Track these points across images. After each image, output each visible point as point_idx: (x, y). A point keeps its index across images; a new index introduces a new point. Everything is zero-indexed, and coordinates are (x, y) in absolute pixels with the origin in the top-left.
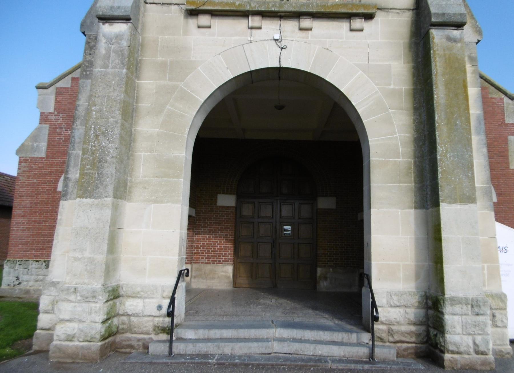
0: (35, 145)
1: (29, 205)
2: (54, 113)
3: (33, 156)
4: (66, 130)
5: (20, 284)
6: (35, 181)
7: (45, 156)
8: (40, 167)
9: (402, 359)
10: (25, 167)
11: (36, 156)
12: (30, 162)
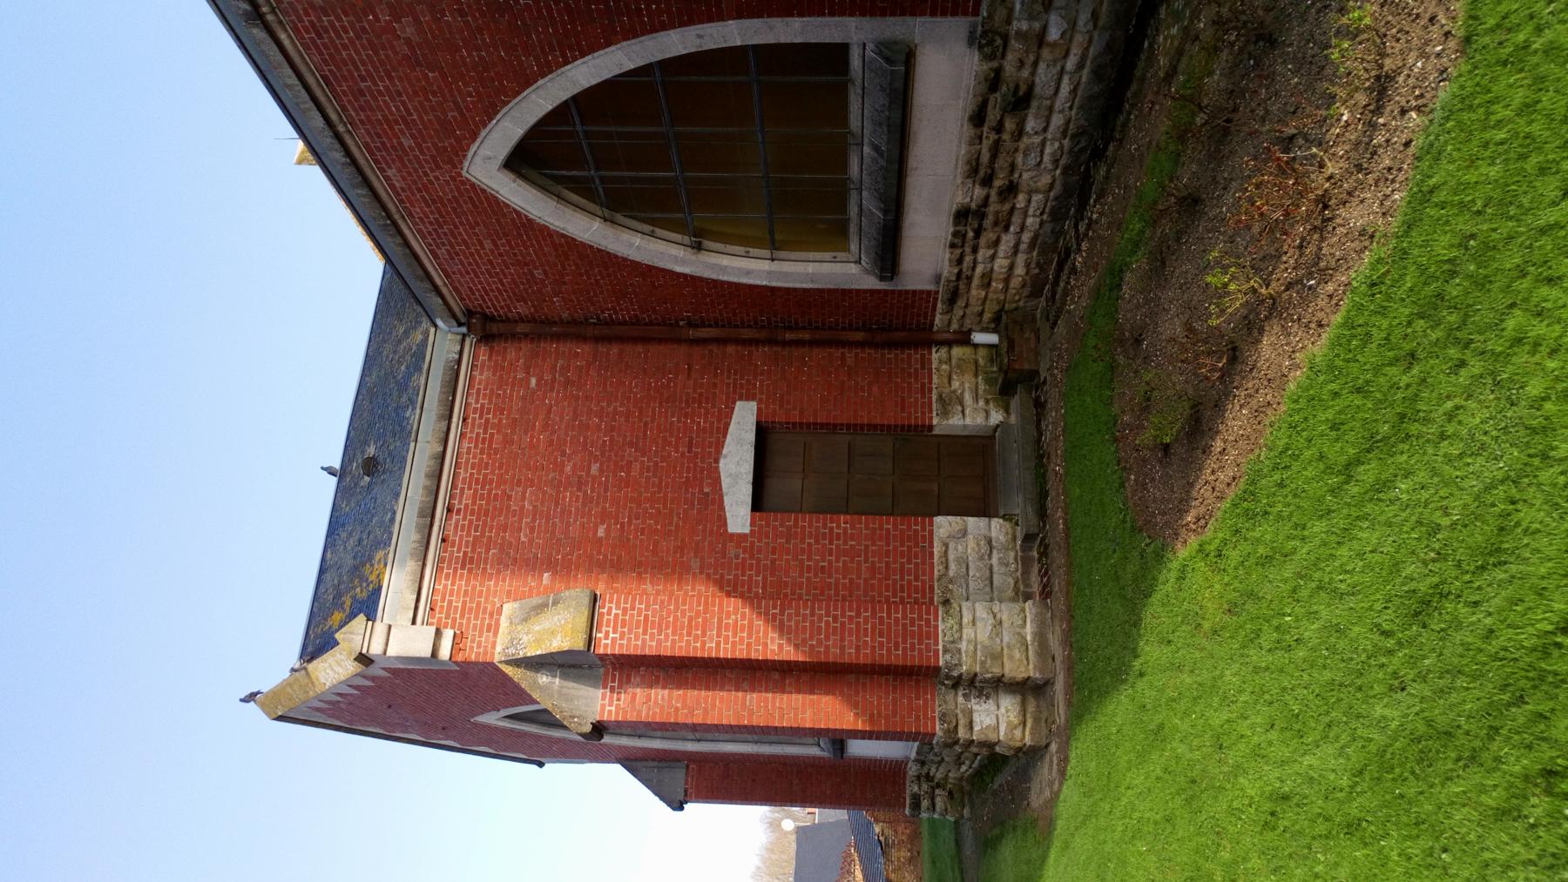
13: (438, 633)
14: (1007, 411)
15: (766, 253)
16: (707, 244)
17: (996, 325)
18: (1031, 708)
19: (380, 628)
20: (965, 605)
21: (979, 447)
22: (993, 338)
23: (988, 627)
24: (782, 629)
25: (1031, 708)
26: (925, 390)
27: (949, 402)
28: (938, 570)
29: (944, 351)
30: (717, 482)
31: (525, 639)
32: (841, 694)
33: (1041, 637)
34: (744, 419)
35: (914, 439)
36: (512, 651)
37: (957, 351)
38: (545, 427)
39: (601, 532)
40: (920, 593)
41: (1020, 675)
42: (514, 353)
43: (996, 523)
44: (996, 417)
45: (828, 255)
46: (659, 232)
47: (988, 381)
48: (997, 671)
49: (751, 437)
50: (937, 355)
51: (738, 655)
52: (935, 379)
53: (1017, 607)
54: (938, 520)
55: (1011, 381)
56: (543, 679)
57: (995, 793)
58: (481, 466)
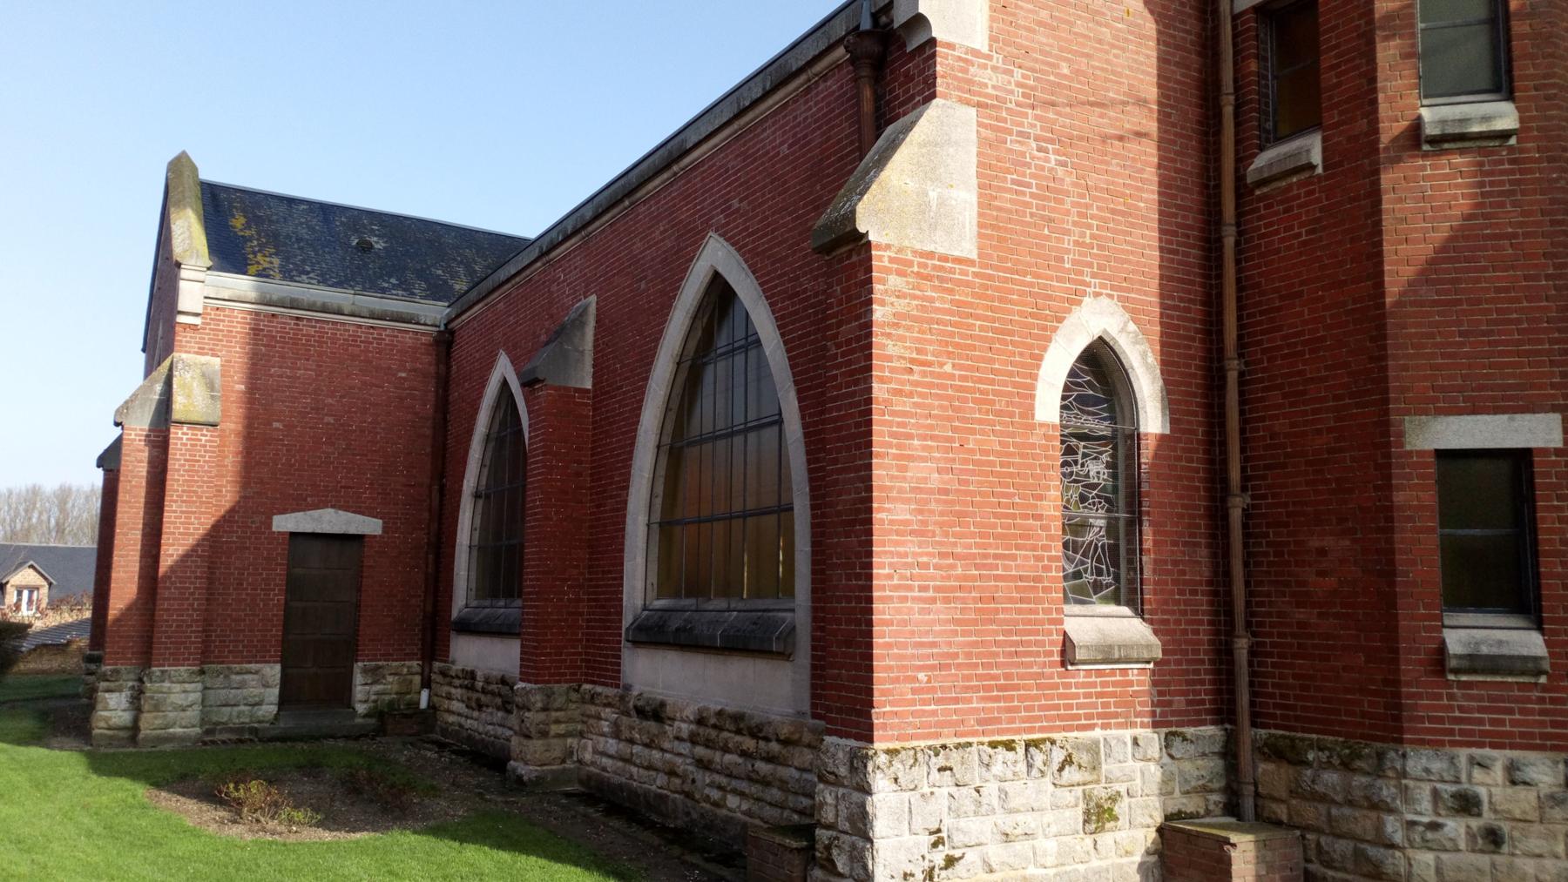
0: (933, 195)
1: (935, 480)
2: (989, 57)
3: (929, 248)
4: (1040, 149)
5: (950, 862)
6: (948, 368)
7: (974, 256)
8: (960, 304)
9: (760, 788)
10: (901, 295)
11: (941, 250)
12: (918, 274)
13: (197, 315)
14: (366, 716)
15: (476, 542)
16: (481, 502)
17: (432, 707)
18: (122, 734)
19: (201, 276)
20: (200, 686)
21: (341, 694)
22: (423, 704)
23: (178, 701)
24: (186, 557)
25: (122, 734)
26: (387, 656)
27: (375, 675)
28: (237, 667)
29: (418, 669)
30: (316, 507)
31: (188, 376)
32: (138, 599)
33: (171, 739)
34: (369, 526)
35: (345, 651)
36: (180, 366)
37: (417, 679)
38: (364, 383)
39: (276, 425)
40: (210, 654)
41: (142, 724)
42: (426, 361)
43: (274, 709)
44: (361, 708)
45: (473, 586)
46: (486, 471)
47: (391, 703)
48: (146, 707)
49: (352, 531)
50: (415, 664)
51: (165, 526)
52: (395, 664)
53: (196, 721)
54: (278, 667)
55: (386, 717)
56: (158, 388)
57: (60, 715)
58: (334, 339)
